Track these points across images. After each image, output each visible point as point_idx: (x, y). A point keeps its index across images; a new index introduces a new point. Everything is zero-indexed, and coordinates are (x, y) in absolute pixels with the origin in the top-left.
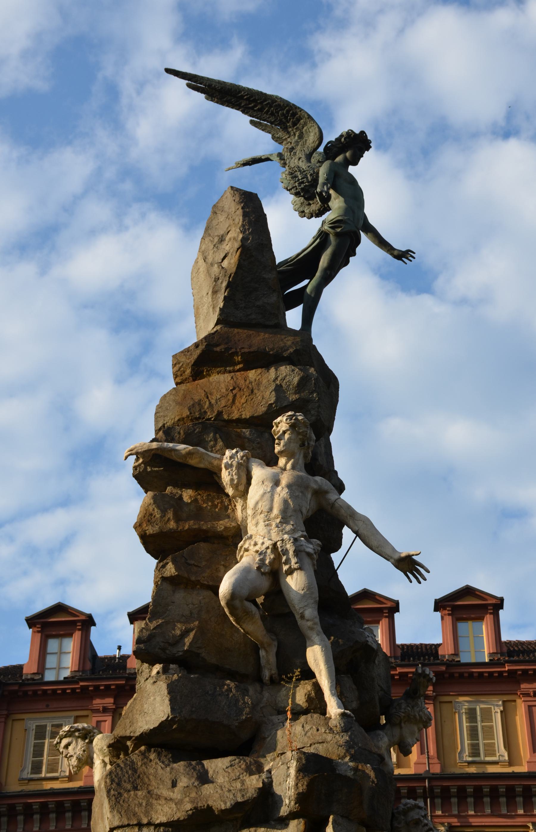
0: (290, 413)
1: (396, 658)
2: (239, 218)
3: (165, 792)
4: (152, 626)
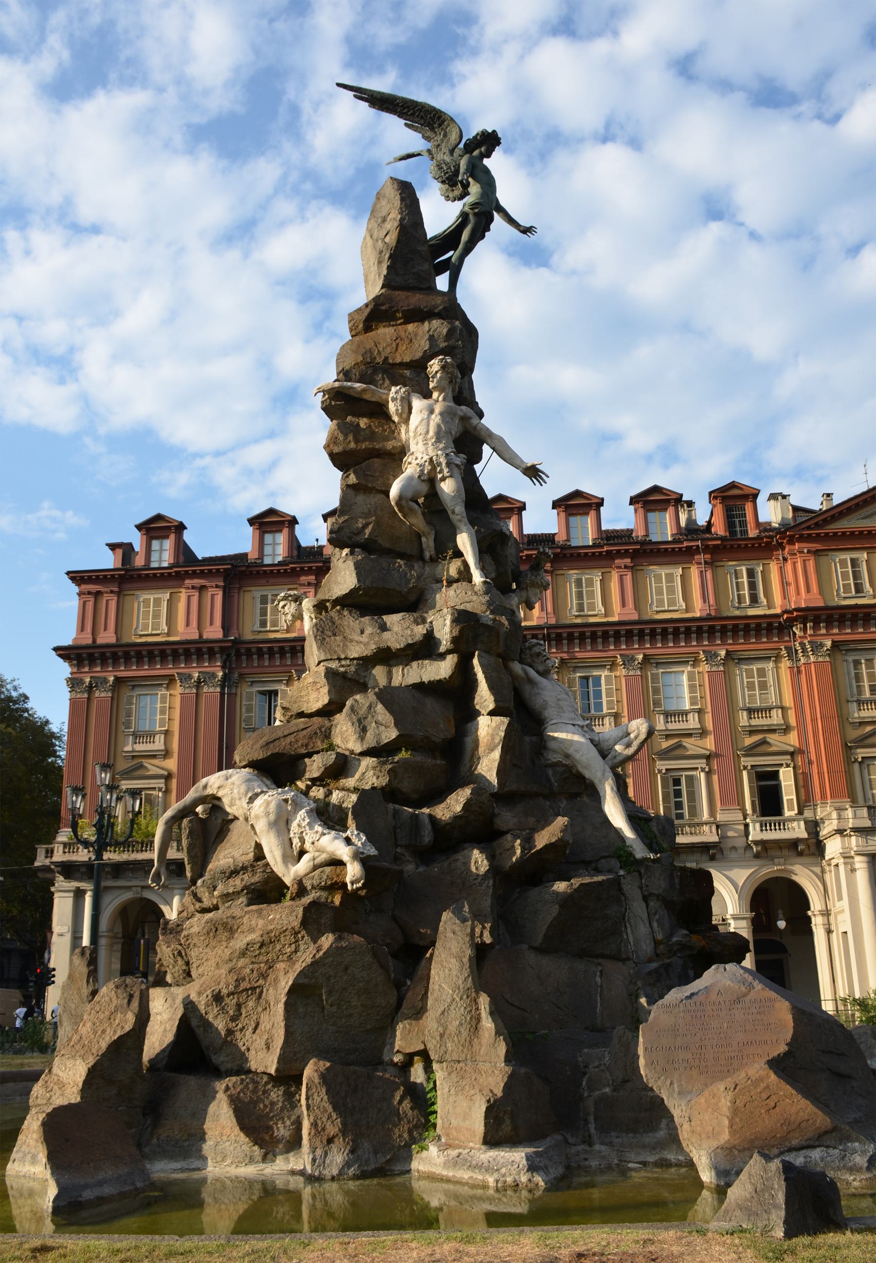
0: (441, 357)
1: (523, 544)
2: (397, 202)
3: (356, 637)
4: (341, 521)
